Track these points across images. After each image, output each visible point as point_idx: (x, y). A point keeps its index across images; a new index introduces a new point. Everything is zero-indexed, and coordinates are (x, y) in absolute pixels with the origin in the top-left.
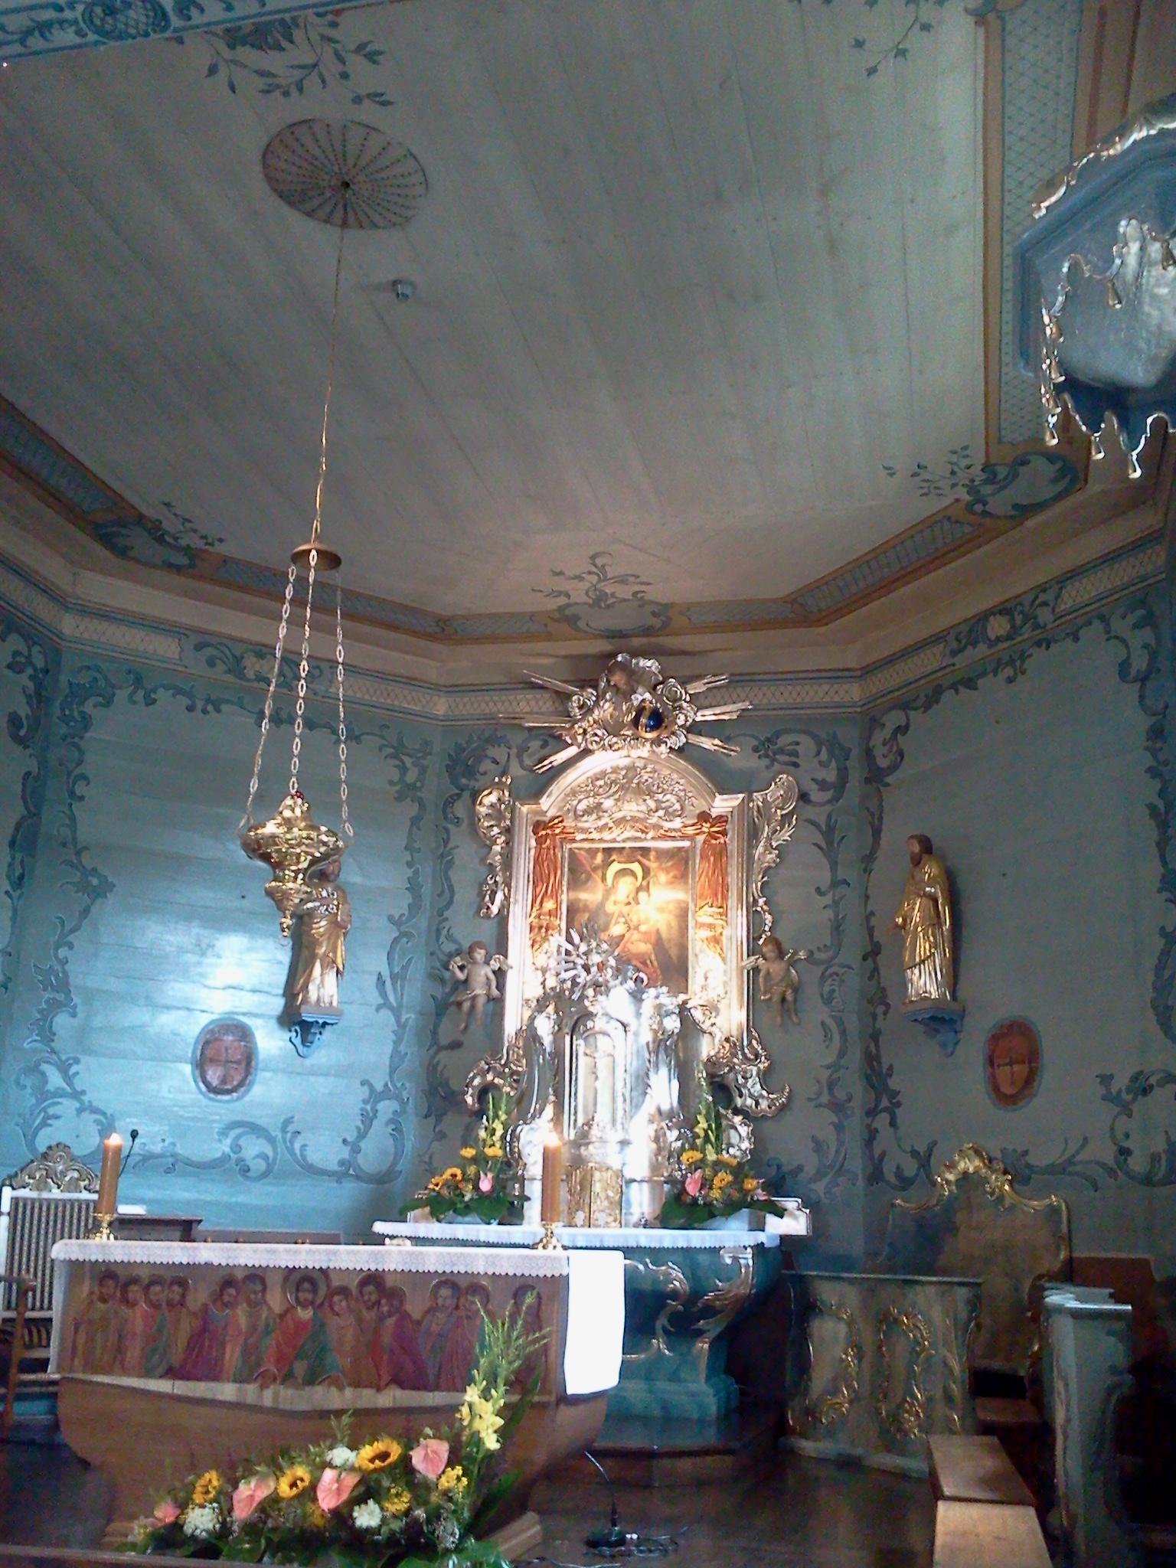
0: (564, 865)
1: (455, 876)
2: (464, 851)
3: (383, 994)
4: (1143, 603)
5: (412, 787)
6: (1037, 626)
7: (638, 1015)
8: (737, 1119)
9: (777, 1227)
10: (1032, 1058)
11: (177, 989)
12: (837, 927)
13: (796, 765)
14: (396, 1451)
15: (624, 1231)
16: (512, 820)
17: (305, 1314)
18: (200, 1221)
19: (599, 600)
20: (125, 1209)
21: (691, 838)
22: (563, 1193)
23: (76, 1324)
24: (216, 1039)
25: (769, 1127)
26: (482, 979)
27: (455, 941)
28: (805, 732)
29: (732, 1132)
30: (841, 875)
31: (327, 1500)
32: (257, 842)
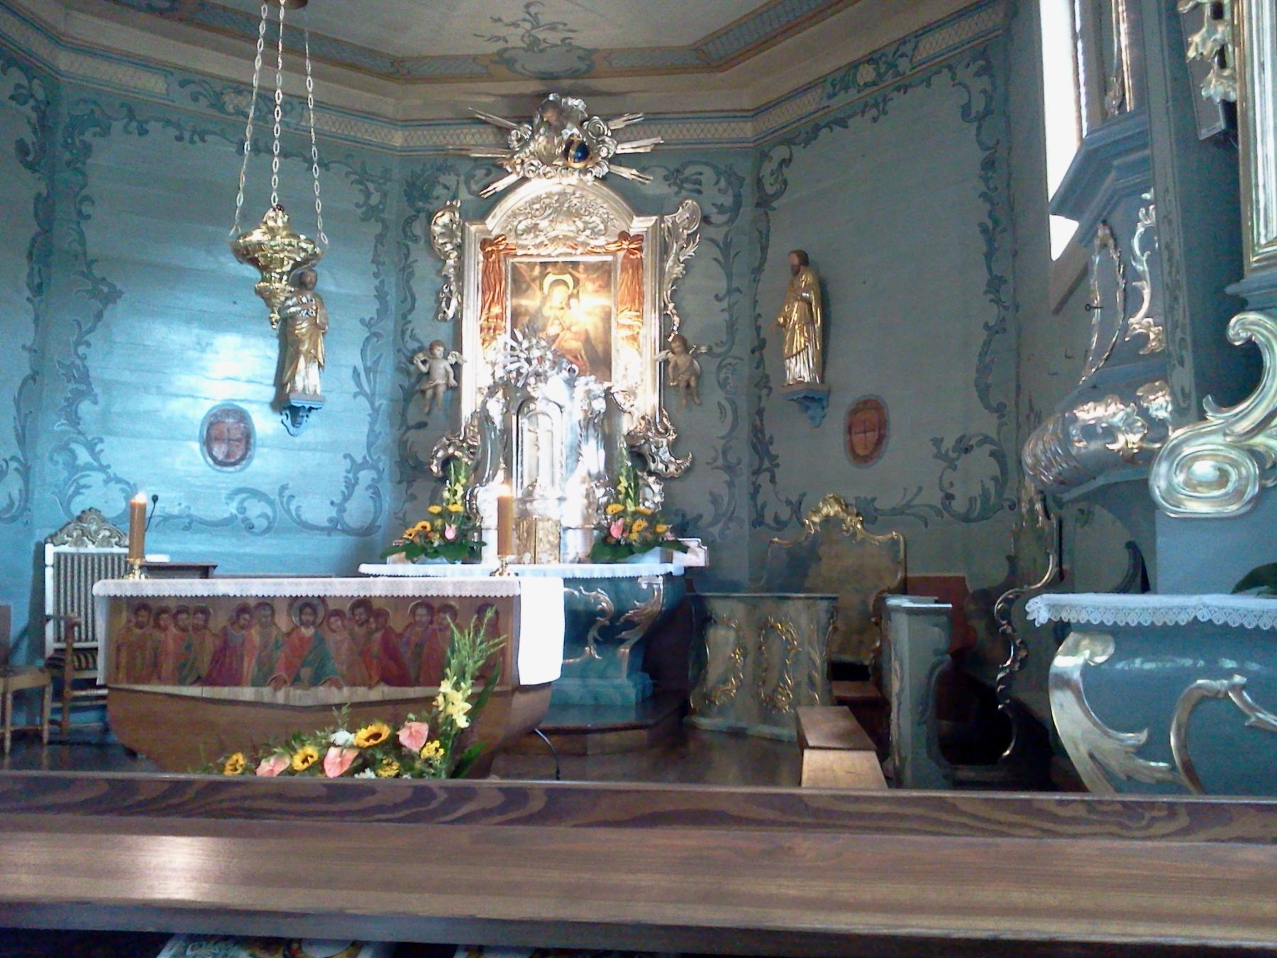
0: (507, 276)
1: (417, 287)
2: (423, 265)
3: (359, 384)
4: (984, 54)
5: (374, 209)
6: (897, 74)
7: (572, 398)
8: (651, 480)
9: (682, 561)
10: (880, 430)
11: (183, 380)
12: (731, 327)
13: (699, 192)
14: (386, 732)
15: (562, 566)
16: (462, 239)
17: (308, 632)
18: (215, 567)
19: (534, 45)
20: (152, 558)
21: (614, 253)
22: (514, 541)
23: (117, 647)
24: (218, 422)
25: (673, 484)
26: (442, 371)
27: (418, 341)
28: (706, 164)
29: (647, 490)
30: (735, 284)
31: (333, 770)
32: (246, 248)
